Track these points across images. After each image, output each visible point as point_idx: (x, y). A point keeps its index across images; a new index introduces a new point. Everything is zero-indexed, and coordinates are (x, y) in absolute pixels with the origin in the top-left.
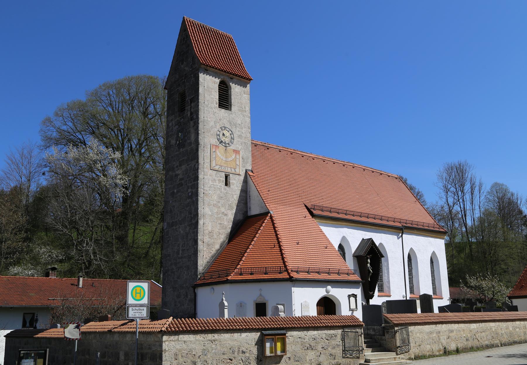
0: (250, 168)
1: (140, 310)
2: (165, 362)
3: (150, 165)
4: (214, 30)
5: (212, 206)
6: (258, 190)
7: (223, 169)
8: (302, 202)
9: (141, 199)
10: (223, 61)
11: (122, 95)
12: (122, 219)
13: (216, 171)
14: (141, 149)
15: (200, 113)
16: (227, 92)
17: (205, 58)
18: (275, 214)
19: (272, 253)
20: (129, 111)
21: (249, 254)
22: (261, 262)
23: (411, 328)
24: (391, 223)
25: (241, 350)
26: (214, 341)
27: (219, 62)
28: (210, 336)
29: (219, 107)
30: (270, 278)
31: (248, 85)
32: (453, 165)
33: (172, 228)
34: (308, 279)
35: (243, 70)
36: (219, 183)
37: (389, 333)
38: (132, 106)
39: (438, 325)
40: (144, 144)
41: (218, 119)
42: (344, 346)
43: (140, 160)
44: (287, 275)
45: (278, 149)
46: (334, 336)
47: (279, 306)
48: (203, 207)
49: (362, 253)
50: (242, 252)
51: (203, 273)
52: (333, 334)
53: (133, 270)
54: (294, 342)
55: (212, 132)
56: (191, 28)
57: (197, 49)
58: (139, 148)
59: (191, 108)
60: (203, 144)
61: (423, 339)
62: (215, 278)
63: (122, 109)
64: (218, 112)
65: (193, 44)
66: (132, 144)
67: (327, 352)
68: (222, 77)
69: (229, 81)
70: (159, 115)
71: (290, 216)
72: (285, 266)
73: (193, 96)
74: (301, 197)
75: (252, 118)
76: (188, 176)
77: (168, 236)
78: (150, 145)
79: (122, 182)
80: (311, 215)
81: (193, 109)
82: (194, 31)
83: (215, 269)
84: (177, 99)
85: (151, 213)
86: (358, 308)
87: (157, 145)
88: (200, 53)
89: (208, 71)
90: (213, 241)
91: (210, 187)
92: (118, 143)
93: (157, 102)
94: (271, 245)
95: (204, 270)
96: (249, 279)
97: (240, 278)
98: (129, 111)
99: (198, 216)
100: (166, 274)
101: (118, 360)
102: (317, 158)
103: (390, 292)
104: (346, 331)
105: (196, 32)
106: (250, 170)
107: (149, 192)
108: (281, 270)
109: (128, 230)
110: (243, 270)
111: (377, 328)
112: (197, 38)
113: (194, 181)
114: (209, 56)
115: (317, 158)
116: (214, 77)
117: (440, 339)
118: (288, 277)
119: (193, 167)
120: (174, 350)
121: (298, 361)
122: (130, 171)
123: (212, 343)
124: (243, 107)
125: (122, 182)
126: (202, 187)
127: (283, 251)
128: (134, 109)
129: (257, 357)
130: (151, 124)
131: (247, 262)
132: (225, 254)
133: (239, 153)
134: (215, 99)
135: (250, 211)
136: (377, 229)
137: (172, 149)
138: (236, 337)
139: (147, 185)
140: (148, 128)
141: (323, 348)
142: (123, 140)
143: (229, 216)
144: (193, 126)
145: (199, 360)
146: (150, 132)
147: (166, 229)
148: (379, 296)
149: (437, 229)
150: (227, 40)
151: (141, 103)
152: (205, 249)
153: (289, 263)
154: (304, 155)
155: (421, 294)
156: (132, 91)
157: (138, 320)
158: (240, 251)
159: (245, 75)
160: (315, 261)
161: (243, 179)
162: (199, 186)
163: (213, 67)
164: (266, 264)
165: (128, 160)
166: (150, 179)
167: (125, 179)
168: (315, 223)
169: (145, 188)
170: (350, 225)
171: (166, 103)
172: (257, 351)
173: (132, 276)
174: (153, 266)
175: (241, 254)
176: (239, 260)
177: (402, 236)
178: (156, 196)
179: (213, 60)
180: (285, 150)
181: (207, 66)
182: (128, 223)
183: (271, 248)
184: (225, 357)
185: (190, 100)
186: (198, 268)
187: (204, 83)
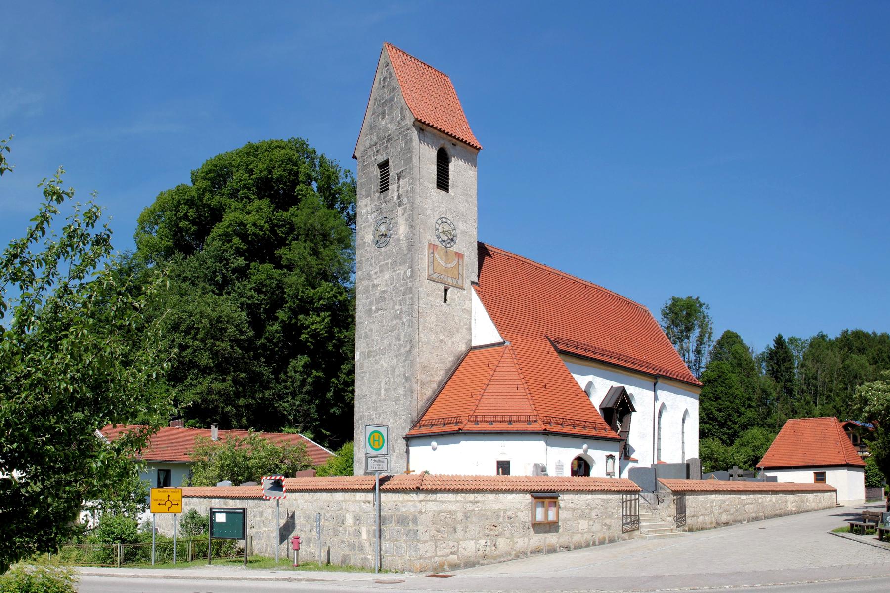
1: (380, 461)
49: (610, 405)
59: (399, 186)
68: (442, 142)
76: (394, 287)
94: (513, 386)
100: (360, 421)
119: (402, 274)
144: (403, 215)
185: (397, 175)
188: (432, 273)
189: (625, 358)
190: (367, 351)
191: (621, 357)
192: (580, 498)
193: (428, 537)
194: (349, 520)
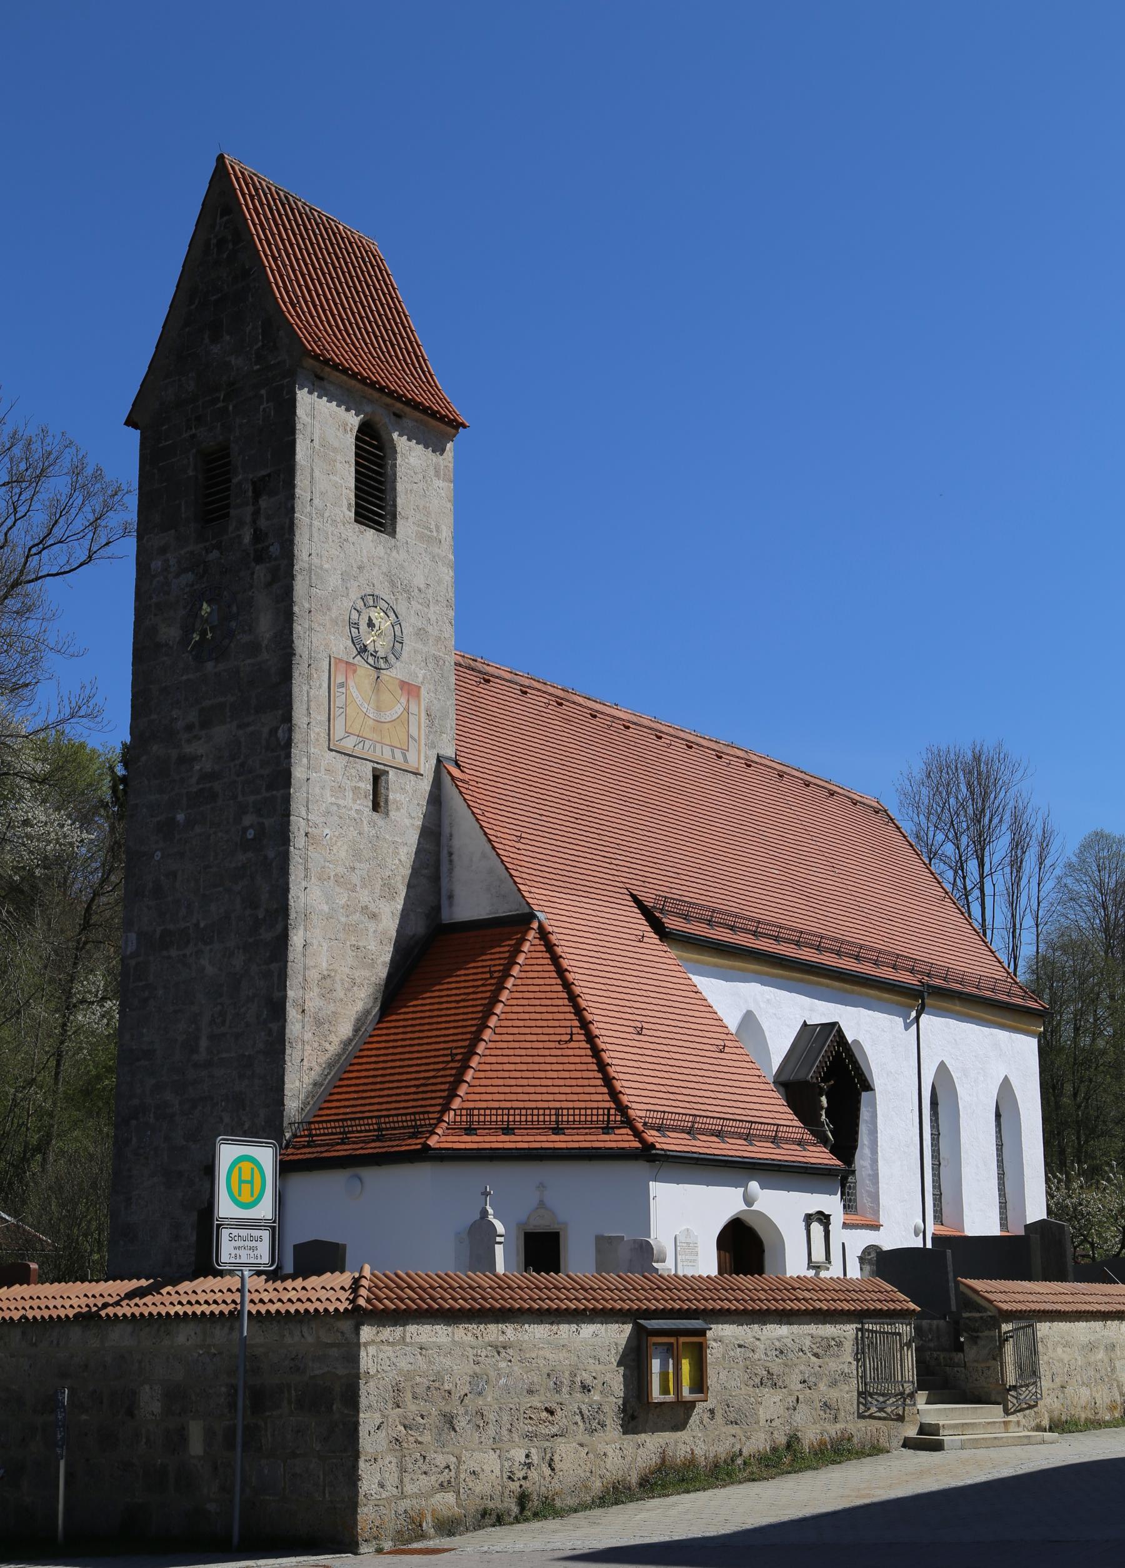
0: (449, 752)
2: (368, 1415)
15: (298, 539)
21: (483, 1060)
23: (1043, 1329)
24: (886, 973)
25: (578, 1379)
26: (504, 1348)
28: (493, 1332)
29: (356, 521)
30: (576, 1145)
31: (449, 446)
32: (952, 756)
33: (165, 953)
36: (354, 801)
37: (981, 1343)
39: (1109, 1322)
41: (355, 566)
42: (864, 1377)
44: (632, 1138)
45: (516, 683)
46: (833, 1343)
48: (304, 884)
52: (833, 1339)
54: (724, 1357)
55: (334, 613)
59: (256, 513)
60: (305, 655)
61: (1073, 1368)
67: (815, 1395)
69: (390, 427)
72: (622, 1109)
75: (460, 567)
76: (242, 765)
84: (191, 473)
86: (832, 1260)
91: (328, 812)
96: (504, 1149)
99: (286, 915)
100: (134, 1122)
101: (130, 1413)
103: (876, 1212)
104: (868, 1330)
108: (608, 1121)
111: (930, 1325)
113: (270, 787)
116: (343, 407)
117: (1113, 1370)
118: (638, 1145)
120: (392, 1376)
121: (736, 1424)
123: (499, 1353)
124: (433, 527)
126: (304, 813)
129: (624, 1404)
133: (418, 696)
134: (344, 491)
135: (451, 905)
136: (846, 991)
137: (165, 658)
138: (564, 1336)
141: (805, 1382)
143: (384, 921)
144: (269, 585)
145: (461, 1410)
148: (845, 1226)
149: (1020, 1002)
152: (308, 1036)
155: (1028, 1223)
157: (246, 1273)
161: (428, 788)
162: (293, 806)
164: (551, 1097)
170: (767, 974)
172: (622, 1387)
177: (917, 1018)
180: (539, 690)
183: (559, 1042)
184: (536, 1401)
185: (254, 483)
186: (286, 1102)
189: (836, 946)
190: (159, 929)
191: (826, 943)
192: (759, 1334)
193: (385, 1443)
194: (150, 1403)
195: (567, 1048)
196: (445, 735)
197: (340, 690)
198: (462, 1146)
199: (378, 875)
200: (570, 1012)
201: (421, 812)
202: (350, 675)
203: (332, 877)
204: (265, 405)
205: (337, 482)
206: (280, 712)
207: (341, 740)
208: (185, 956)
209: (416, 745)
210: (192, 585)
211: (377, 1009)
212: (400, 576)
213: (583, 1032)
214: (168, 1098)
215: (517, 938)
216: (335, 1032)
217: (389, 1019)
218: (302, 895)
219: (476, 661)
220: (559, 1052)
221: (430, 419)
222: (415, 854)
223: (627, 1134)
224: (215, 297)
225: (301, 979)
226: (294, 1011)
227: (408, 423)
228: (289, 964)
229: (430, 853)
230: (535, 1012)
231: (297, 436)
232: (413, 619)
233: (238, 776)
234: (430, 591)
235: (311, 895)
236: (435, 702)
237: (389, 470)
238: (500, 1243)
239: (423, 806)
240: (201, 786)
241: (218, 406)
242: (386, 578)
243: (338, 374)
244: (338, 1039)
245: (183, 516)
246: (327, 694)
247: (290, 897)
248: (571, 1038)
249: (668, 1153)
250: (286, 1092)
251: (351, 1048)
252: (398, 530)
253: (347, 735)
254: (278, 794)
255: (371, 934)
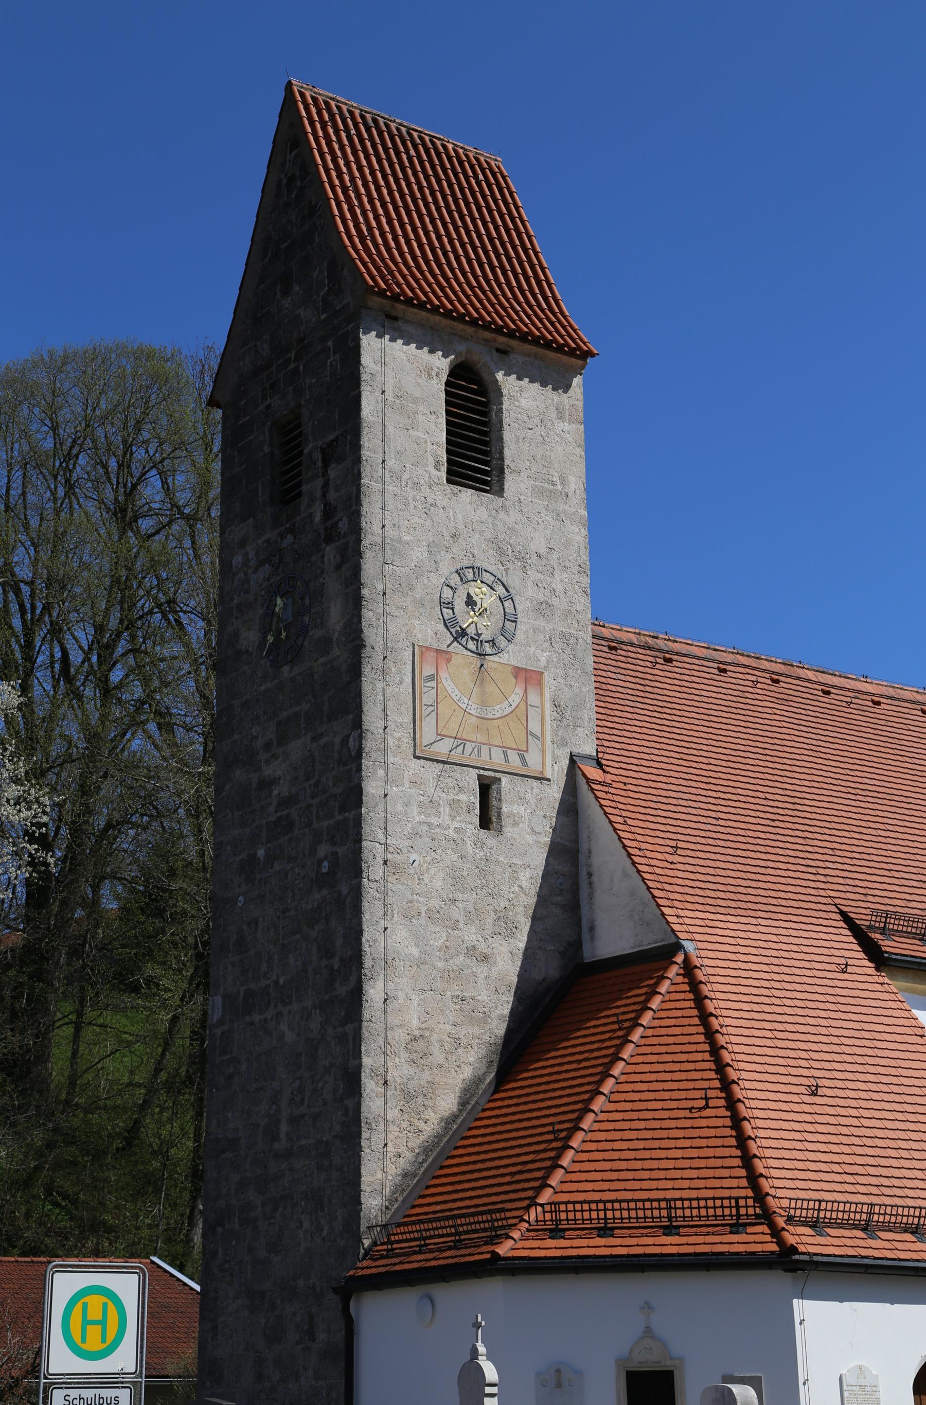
0: (589, 748)
3: (150, 737)
4: (421, 138)
5: (423, 919)
6: (624, 847)
7: (468, 754)
8: (829, 901)
9: (106, 889)
10: (464, 274)
11: (25, 433)
12: (24, 978)
13: (438, 761)
14: (110, 670)
15: (365, 509)
16: (485, 414)
17: (387, 267)
18: (703, 953)
19: (696, 1133)
20: (55, 503)
21: (590, 1136)
22: (646, 1175)
27: (447, 280)
29: (449, 481)
30: (690, 1249)
31: (577, 381)
33: (248, 1019)
34: (866, 1261)
35: (554, 314)
36: (453, 818)
38: (67, 481)
40: (122, 646)
41: (446, 534)
43: (104, 717)
44: (768, 1238)
45: (713, 661)
47: (736, 1389)
48: (382, 924)
50: (557, 1127)
51: (384, 1226)
53: (69, 1212)
55: (419, 593)
56: (321, 133)
57: (351, 224)
58: (100, 663)
59: (326, 485)
60: (379, 646)
62: (440, 1250)
63: (24, 494)
64: (445, 503)
65: (333, 202)
66: (70, 645)
68: (462, 347)
69: (492, 366)
70: (187, 518)
71: (776, 961)
72: (760, 1197)
73: (336, 434)
74: (822, 878)
76: (316, 785)
77: (226, 1058)
78: (146, 652)
79: (25, 814)
80: (870, 960)
81: (336, 490)
82: (336, 146)
83: (438, 1208)
84: (267, 449)
85: (150, 950)
87: (176, 649)
88: (363, 241)
89: (400, 323)
90: (427, 1076)
91: (415, 834)
92: (8, 642)
93: (176, 461)
95: (390, 1213)
96: (595, 1256)
97: (552, 1248)
98: (55, 501)
99: (360, 964)
100: (220, 1229)
102: (891, 698)
105: (342, 147)
106: (589, 757)
107: (141, 856)
108: (738, 1215)
109: (50, 1027)
110: (567, 1211)
112: (347, 178)
113: (342, 809)
114: (402, 254)
115: (891, 698)
116: (426, 349)
118: (774, 1248)
119: (337, 747)
122: (61, 765)
125: (25, 814)
127: (751, 1143)
128: (74, 494)
130: (152, 559)
131: (584, 1176)
132: (483, 1135)
133: (540, 684)
134: (430, 447)
135: (592, 939)
137: (246, 667)
139: (135, 826)
140: (136, 577)
142: (29, 632)
144: (338, 567)
146: (148, 592)
147: (221, 1022)
150: (479, 183)
151: (105, 466)
152: (393, 1114)
153: (777, 1183)
154: (833, 687)
156: (64, 414)
158: (552, 1124)
159: (562, 337)
160: (896, 1173)
161: (558, 796)
162: (366, 828)
163: (422, 306)
164: (669, 1184)
165: (50, 718)
166: (150, 799)
167: (37, 801)
168: (893, 997)
169: (126, 839)
171: (217, 466)
173: (67, 1239)
174: (157, 1191)
175: (556, 1140)
176: (548, 1164)
178: (172, 873)
179: (422, 272)
181: (395, 298)
182: (51, 997)
183: (691, 1109)
186: (363, 1200)
187: (383, 374)
188: (433, 737)
190: (242, 989)
195: (701, 1117)
196: (582, 729)
197: (429, 684)
198: (542, 1253)
199: (490, 907)
200: (710, 1070)
201: (548, 825)
202: (442, 665)
203: (423, 914)
204: (332, 359)
205: (419, 438)
206: (351, 717)
207: (431, 744)
208: (265, 1020)
209: (539, 744)
210: (269, 579)
211: (492, 1075)
212: (511, 542)
213: (723, 1095)
214: (252, 1198)
215: (658, 976)
216: (432, 1108)
217: (506, 1087)
218: (380, 938)
219: (657, 638)
220: (688, 1123)
221: (547, 352)
222: (543, 877)
223: (763, 1233)
224: (286, 244)
225: (381, 1042)
226: (373, 1083)
227: (516, 359)
228: (365, 1024)
229: (564, 875)
230: (665, 1072)
231: (362, 388)
232: (531, 592)
233: (313, 798)
234: (555, 556)
235: (394, 937)
236: (566, 689)
237: (494, 417)
238: (492, 1395)
239: (551, 818)
240: (279, 814)
241: (289, 368)
242: (491, 545)
243: (416, 311)
244: (438, 1116)
245: (260, 500)
246: (411, 690)
247: (364, 940)
248: (707, 1104)
249: (815, 1258)
250: (363, 1187)
251: (455, 1126)
252: (506, 487)
253: (439, 738)
254: (350, 815)
255: (481, 980)
